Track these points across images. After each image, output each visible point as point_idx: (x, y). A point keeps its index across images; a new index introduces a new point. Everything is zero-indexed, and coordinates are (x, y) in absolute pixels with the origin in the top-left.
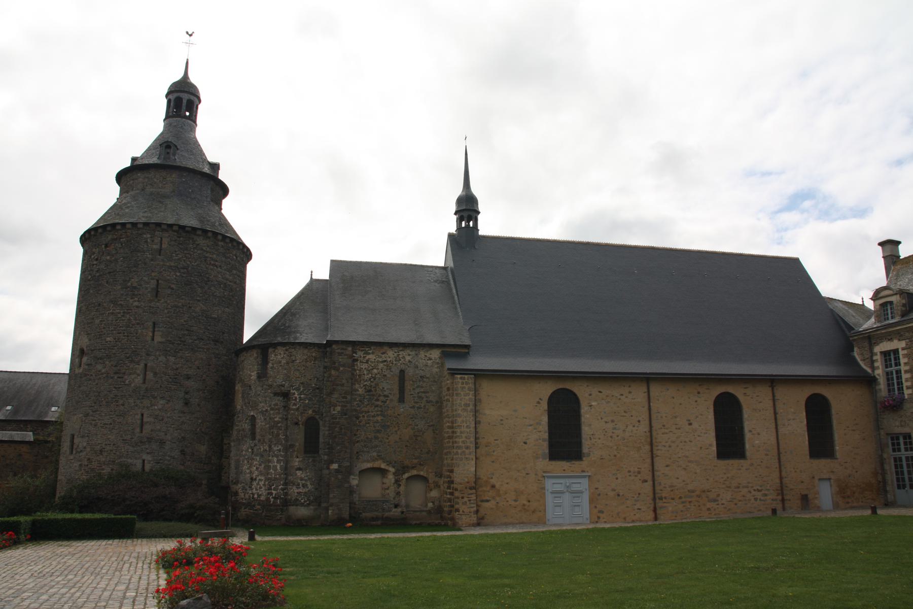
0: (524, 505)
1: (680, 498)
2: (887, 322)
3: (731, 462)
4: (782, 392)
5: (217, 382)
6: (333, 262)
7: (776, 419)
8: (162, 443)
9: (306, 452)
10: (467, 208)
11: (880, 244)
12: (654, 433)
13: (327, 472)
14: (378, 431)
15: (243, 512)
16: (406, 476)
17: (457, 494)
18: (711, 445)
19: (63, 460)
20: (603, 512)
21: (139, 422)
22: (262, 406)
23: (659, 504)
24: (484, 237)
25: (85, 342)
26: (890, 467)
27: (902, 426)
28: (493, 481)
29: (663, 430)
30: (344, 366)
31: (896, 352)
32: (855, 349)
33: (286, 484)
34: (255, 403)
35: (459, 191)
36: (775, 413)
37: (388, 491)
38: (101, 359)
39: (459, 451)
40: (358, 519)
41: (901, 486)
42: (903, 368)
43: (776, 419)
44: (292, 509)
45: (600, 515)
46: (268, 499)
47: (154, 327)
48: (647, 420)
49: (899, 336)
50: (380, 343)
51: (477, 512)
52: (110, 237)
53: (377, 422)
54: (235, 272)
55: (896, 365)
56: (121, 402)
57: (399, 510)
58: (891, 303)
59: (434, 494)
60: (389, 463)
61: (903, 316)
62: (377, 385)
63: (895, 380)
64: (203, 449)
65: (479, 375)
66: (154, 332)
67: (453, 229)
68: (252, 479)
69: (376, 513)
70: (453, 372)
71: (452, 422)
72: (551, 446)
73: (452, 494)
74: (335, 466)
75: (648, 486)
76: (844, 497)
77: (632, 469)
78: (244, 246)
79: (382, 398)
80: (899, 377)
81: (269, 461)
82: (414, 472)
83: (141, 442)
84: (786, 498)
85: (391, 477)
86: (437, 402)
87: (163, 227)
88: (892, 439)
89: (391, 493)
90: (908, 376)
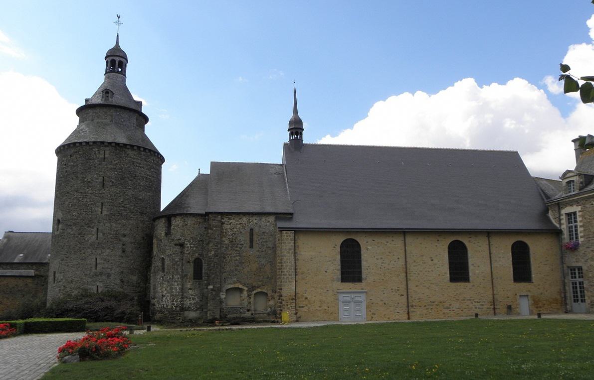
0: (325, 310)
1: (425, 306)
2: (570, 194)
3: (459, 284)
4: (496, 241)
5: (143, 238)
6: (211, 162)
7: (490, 257)
8: (109, 275)
9: (194, 279)
10: (296, 128)
11: (573, 141)
12: (408, 266)
13: (206, 290)
14: (238, 266)
15: (158, 316)
16: (254, 292)
17: (283, 303)
18: (446, 273)
19: (49, 287)
20: (375, 314)
21: (94, 263)
22: (168, 252)
23: (411, 309)
24: (306, 145)
25: (60, 216)
26: (569, 289)
27: (577, 262)
28: (306, 295)
29: (415, 264)
30: (216, 227)
31: (575, 213)
32: (550, 211)
33: (182, 298)
34: (164, 251)
35: (290, 116)
36: (490, 254)
37: (243, 302)
38: (70, 225)
39: (285, 277)
40: (224, 319)
41: (576, 301)
42: (579, 224)
43: (490, 257)
44: (186, 313)
45: (373, 316)
46: (172, 308)
47: (102, 206)
48: (404, 258)
49: (577, 203)
50: (238, 213)
51: (296, 313)
52: (72, 151)
53: (237, 260)
54: (153, 170)
55: (575, 222)
56: (83, 251)
57: (250, 312)
58: (573, 181)
59: (272, 303)
60: (244, 285)
61: (580, 190)
62: (236, 238)
63: (573, 232)
64: (134, 278)
65: (297, 231)
66: (102, 208)
67: (287, 140)
68: (163, 295)
69: (236, 315)
70: (282, 230)
71: (281, 260)
72: (342, 273)
73: (281, 303)
74: (211, 287)
75: (404, 299)
76: (537, 307)
77: (394, 288)
78: (159, 154)
79: (239, 246)
80: (576, 230)
81: (173, 285)
82: (259, 290)
83: (96, 275)
84: (496, 307)
85: (245, 293)
86: (273, 248)
87: (105, 144)
88: (571, 270)
89: (245, 303)
90: (582, 229)
